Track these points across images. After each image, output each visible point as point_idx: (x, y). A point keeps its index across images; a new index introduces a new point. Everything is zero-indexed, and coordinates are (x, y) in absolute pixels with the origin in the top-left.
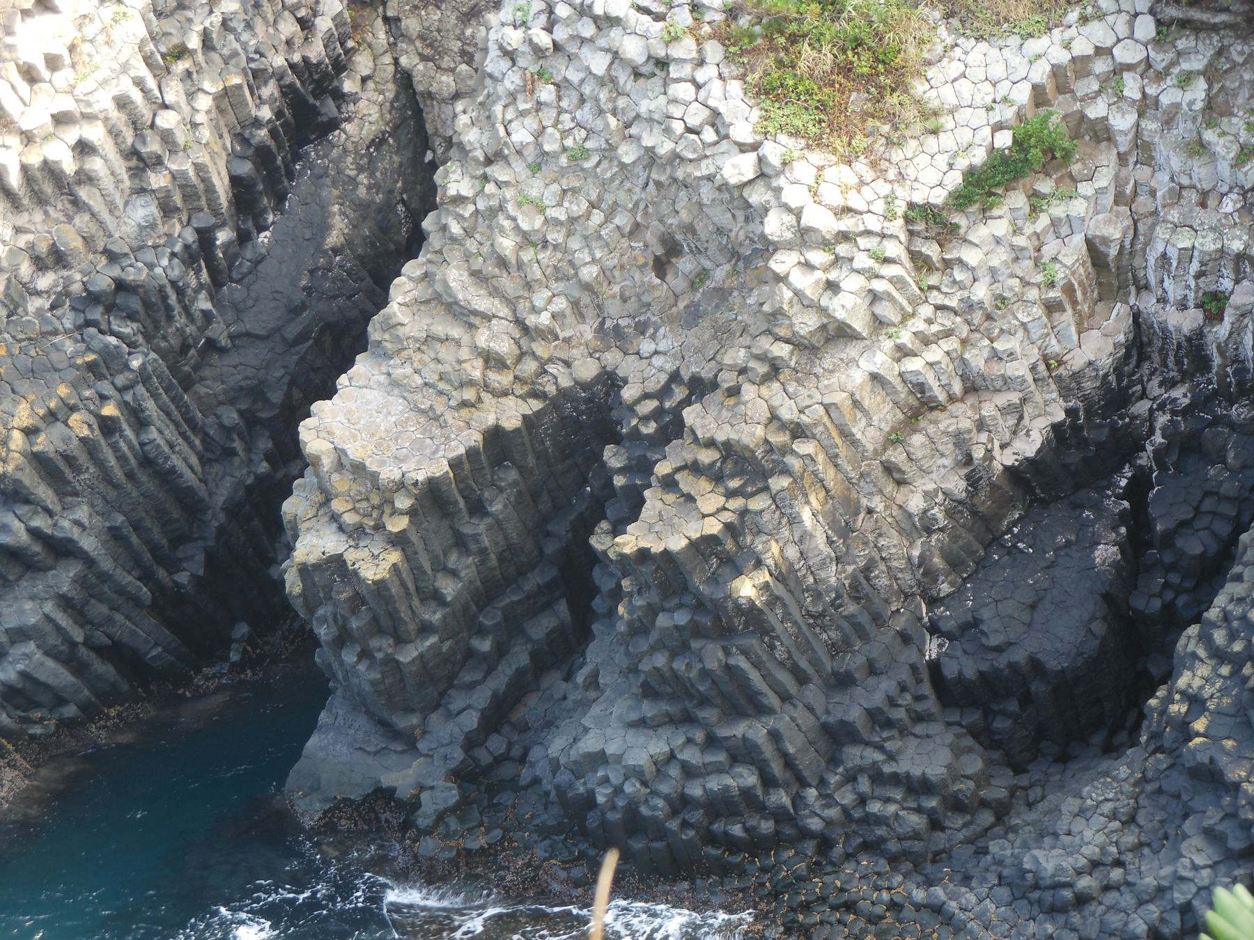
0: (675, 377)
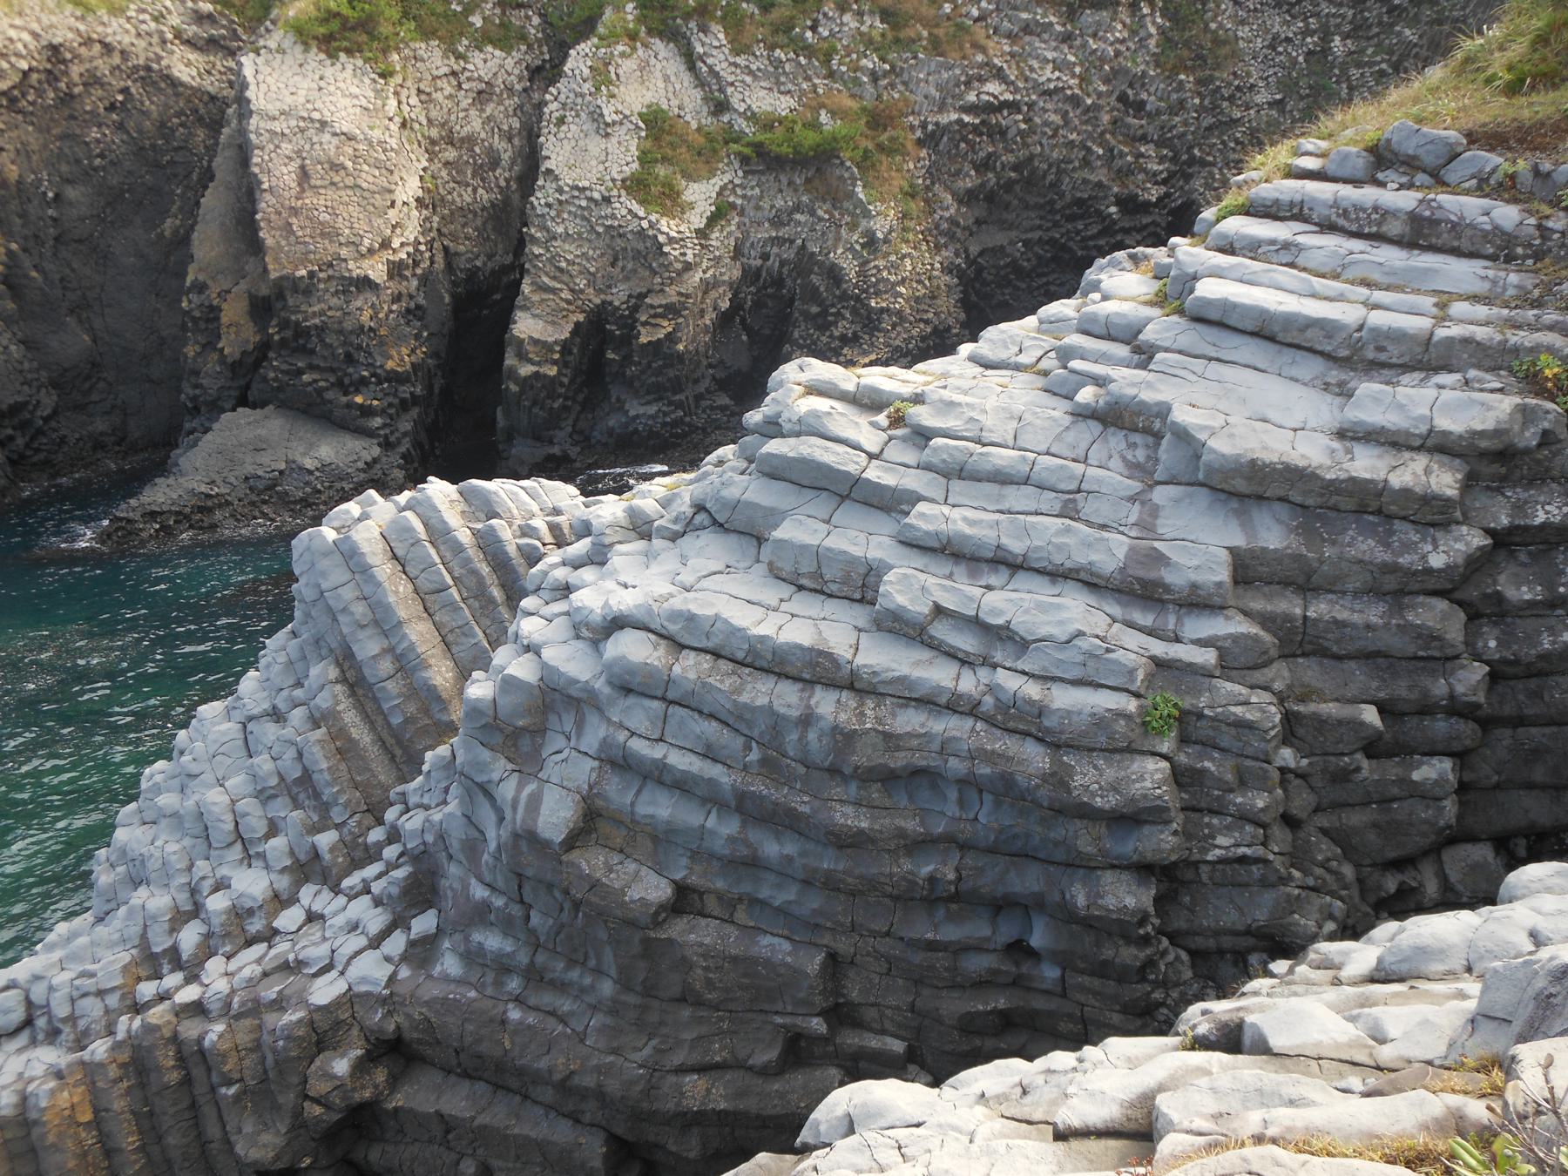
0: (630, 296)
